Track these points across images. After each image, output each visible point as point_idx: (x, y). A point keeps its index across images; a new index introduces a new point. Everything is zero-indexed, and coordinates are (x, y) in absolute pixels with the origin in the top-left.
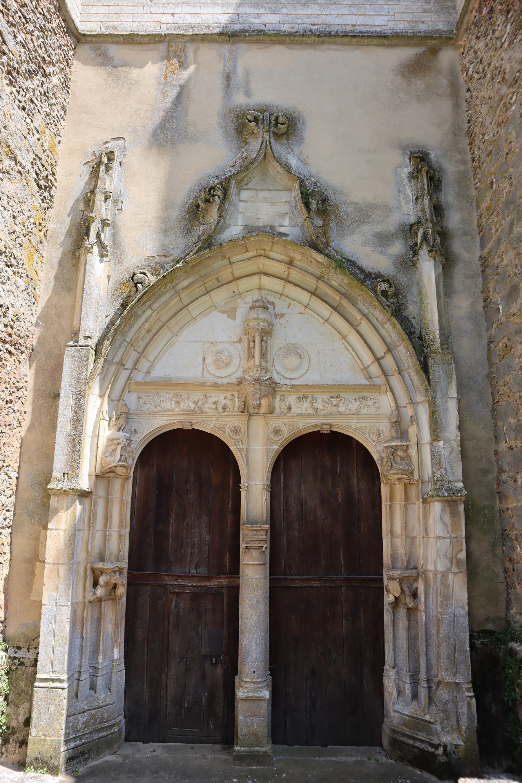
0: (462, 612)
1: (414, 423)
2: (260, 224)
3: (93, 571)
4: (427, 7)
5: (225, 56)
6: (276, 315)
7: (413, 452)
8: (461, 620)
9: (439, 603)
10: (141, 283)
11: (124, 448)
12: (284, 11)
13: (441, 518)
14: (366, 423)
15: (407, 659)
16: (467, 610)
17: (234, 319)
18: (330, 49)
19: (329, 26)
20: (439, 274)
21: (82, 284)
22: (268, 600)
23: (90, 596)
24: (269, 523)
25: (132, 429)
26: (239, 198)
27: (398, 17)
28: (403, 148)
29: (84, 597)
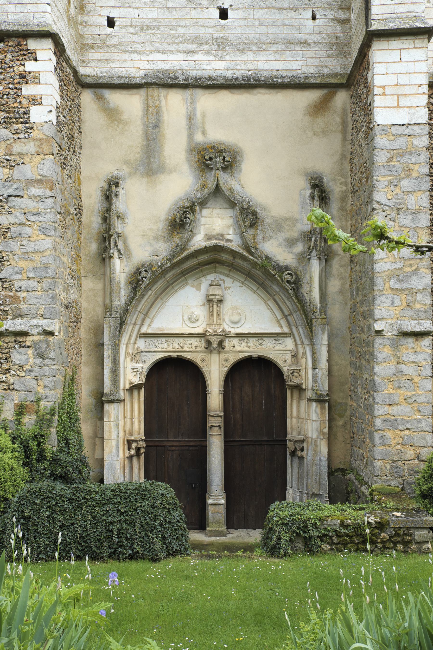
0: (324, 459)
2: (214, 233)
3: (128, 440)
4: (330, 52)
5: (187, 100)
6: (225, 288)
7: (303, 373)
10: (145, 277)
12: (228, 58)
14: (280, 352)
17: (200, 291)
18: (260, 93)
19: (260, 71)
22: (223, 453)
23: (127, 455)
27: (310, 61)
29: (124, 455)
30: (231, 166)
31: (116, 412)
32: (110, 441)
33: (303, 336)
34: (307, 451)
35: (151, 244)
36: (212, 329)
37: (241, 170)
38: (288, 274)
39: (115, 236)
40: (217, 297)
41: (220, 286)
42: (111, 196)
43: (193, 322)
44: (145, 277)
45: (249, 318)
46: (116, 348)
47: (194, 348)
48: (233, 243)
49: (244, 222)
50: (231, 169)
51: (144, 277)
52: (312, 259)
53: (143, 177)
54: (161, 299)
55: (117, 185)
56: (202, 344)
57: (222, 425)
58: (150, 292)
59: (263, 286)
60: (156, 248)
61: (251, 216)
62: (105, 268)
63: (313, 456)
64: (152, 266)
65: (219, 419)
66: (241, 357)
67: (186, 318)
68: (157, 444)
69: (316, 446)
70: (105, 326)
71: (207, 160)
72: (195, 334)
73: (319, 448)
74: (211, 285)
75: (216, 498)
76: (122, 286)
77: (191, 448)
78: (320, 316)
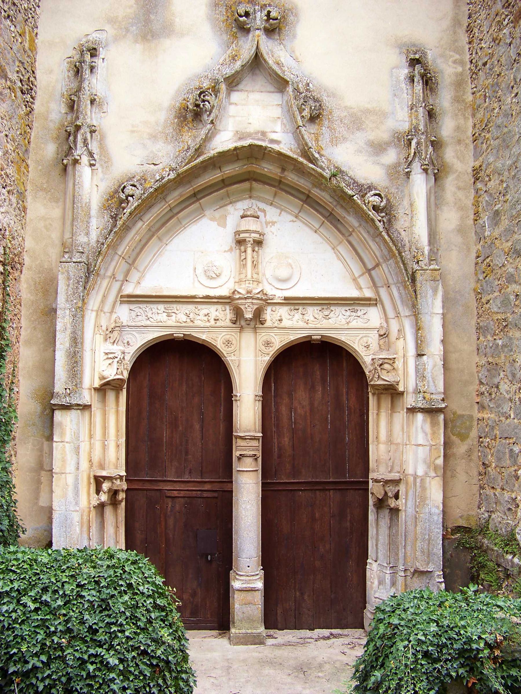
0: (437, 511)
1: (402, 336)
6: (267, 223)
7: (399, 364)
8: (436, 518)
9: (418, 504)
10: (132, 196)
11: (120, 362)
13: (422, 428)
14: (358, 333)
15: (388, 553)
16: (441, 509)
17: (224, 226)
20: (430, 188)
21: (71, 197)
23: (95, 502)
24: (261, 431)
25: (126, 342)
26: (229, 101)
28: (400, 47)
30: (280, 29)
31: (75, 426)
32: (63, 475)
33: (399, 303)
34: (406, 499)
35: (144, 146)
36: (244, 289)
37: (294, 36)
38: (375, 195)
39: (84, 130)
40: (253, 235)
41: (258, 217)
42: (82, 68)
43: (212, 278)
44: (132, 196)
45: (304, 272)
46: (79, 313)
47: (212, 322)
48: (282, 146)
49: (301, 110)
50: (279, 33)
51: (129, 196)
52: (413, 173)
53: (136, 41)
54: (160, 239)
55: (93, 52)
56: (225, 315)
57: (259, 454)
58: (140, 224)
59: (332, 218)
60: (152, 152)
61: (311, 103)
62: (65, 182)
63: (416, 506)
64: (145, 180)
65: (255, 443)
66: (292, 338)
67: (200, 271)
68: (147, 486)
69: (423, 488)
70: (60, 277)
71: (241, 16)
72: (215, 298)
73: (428, 491)
74: (242, 217)
75: (248, 577)
76: (94, 211)
77: (205, 495)
78: (430, 265)
